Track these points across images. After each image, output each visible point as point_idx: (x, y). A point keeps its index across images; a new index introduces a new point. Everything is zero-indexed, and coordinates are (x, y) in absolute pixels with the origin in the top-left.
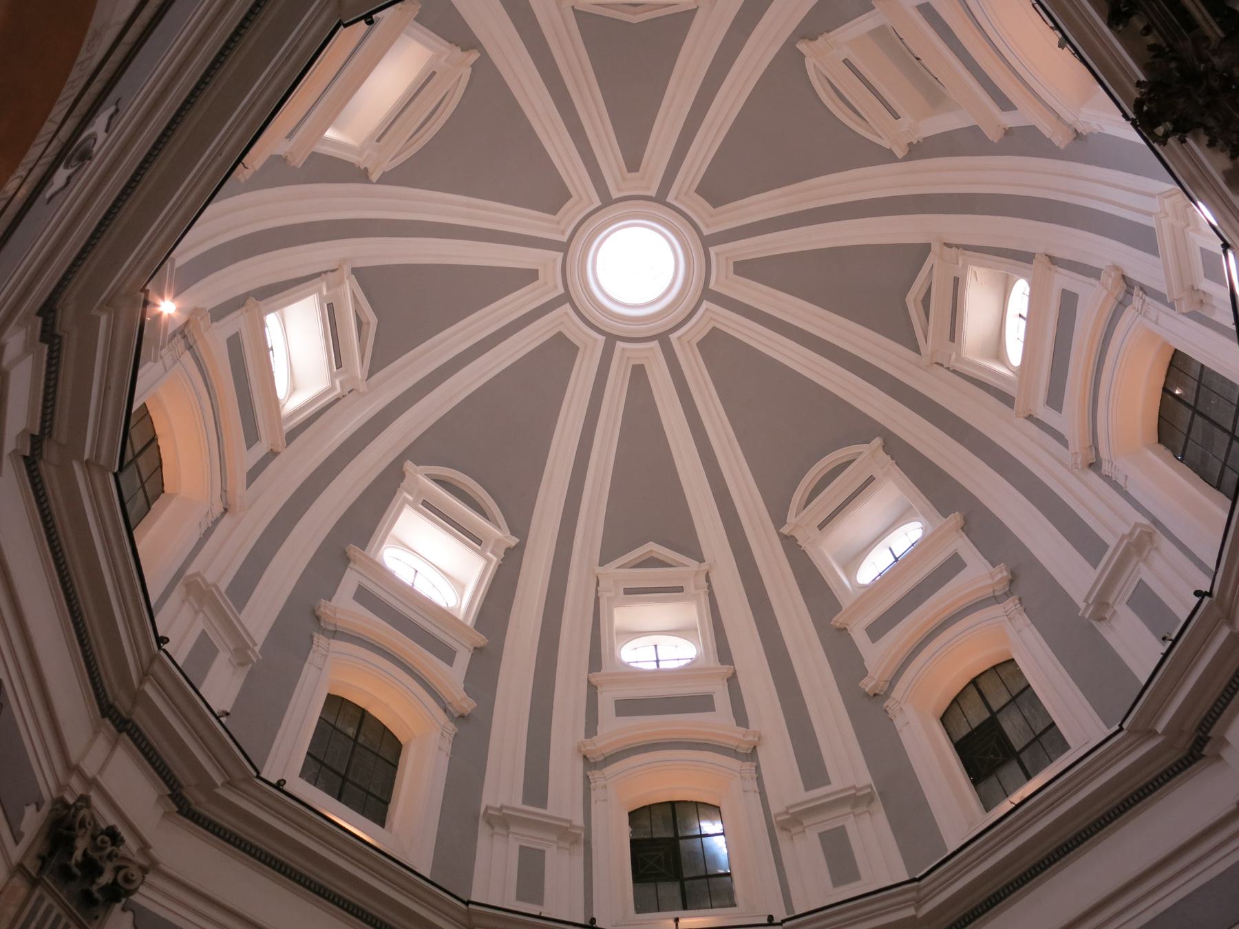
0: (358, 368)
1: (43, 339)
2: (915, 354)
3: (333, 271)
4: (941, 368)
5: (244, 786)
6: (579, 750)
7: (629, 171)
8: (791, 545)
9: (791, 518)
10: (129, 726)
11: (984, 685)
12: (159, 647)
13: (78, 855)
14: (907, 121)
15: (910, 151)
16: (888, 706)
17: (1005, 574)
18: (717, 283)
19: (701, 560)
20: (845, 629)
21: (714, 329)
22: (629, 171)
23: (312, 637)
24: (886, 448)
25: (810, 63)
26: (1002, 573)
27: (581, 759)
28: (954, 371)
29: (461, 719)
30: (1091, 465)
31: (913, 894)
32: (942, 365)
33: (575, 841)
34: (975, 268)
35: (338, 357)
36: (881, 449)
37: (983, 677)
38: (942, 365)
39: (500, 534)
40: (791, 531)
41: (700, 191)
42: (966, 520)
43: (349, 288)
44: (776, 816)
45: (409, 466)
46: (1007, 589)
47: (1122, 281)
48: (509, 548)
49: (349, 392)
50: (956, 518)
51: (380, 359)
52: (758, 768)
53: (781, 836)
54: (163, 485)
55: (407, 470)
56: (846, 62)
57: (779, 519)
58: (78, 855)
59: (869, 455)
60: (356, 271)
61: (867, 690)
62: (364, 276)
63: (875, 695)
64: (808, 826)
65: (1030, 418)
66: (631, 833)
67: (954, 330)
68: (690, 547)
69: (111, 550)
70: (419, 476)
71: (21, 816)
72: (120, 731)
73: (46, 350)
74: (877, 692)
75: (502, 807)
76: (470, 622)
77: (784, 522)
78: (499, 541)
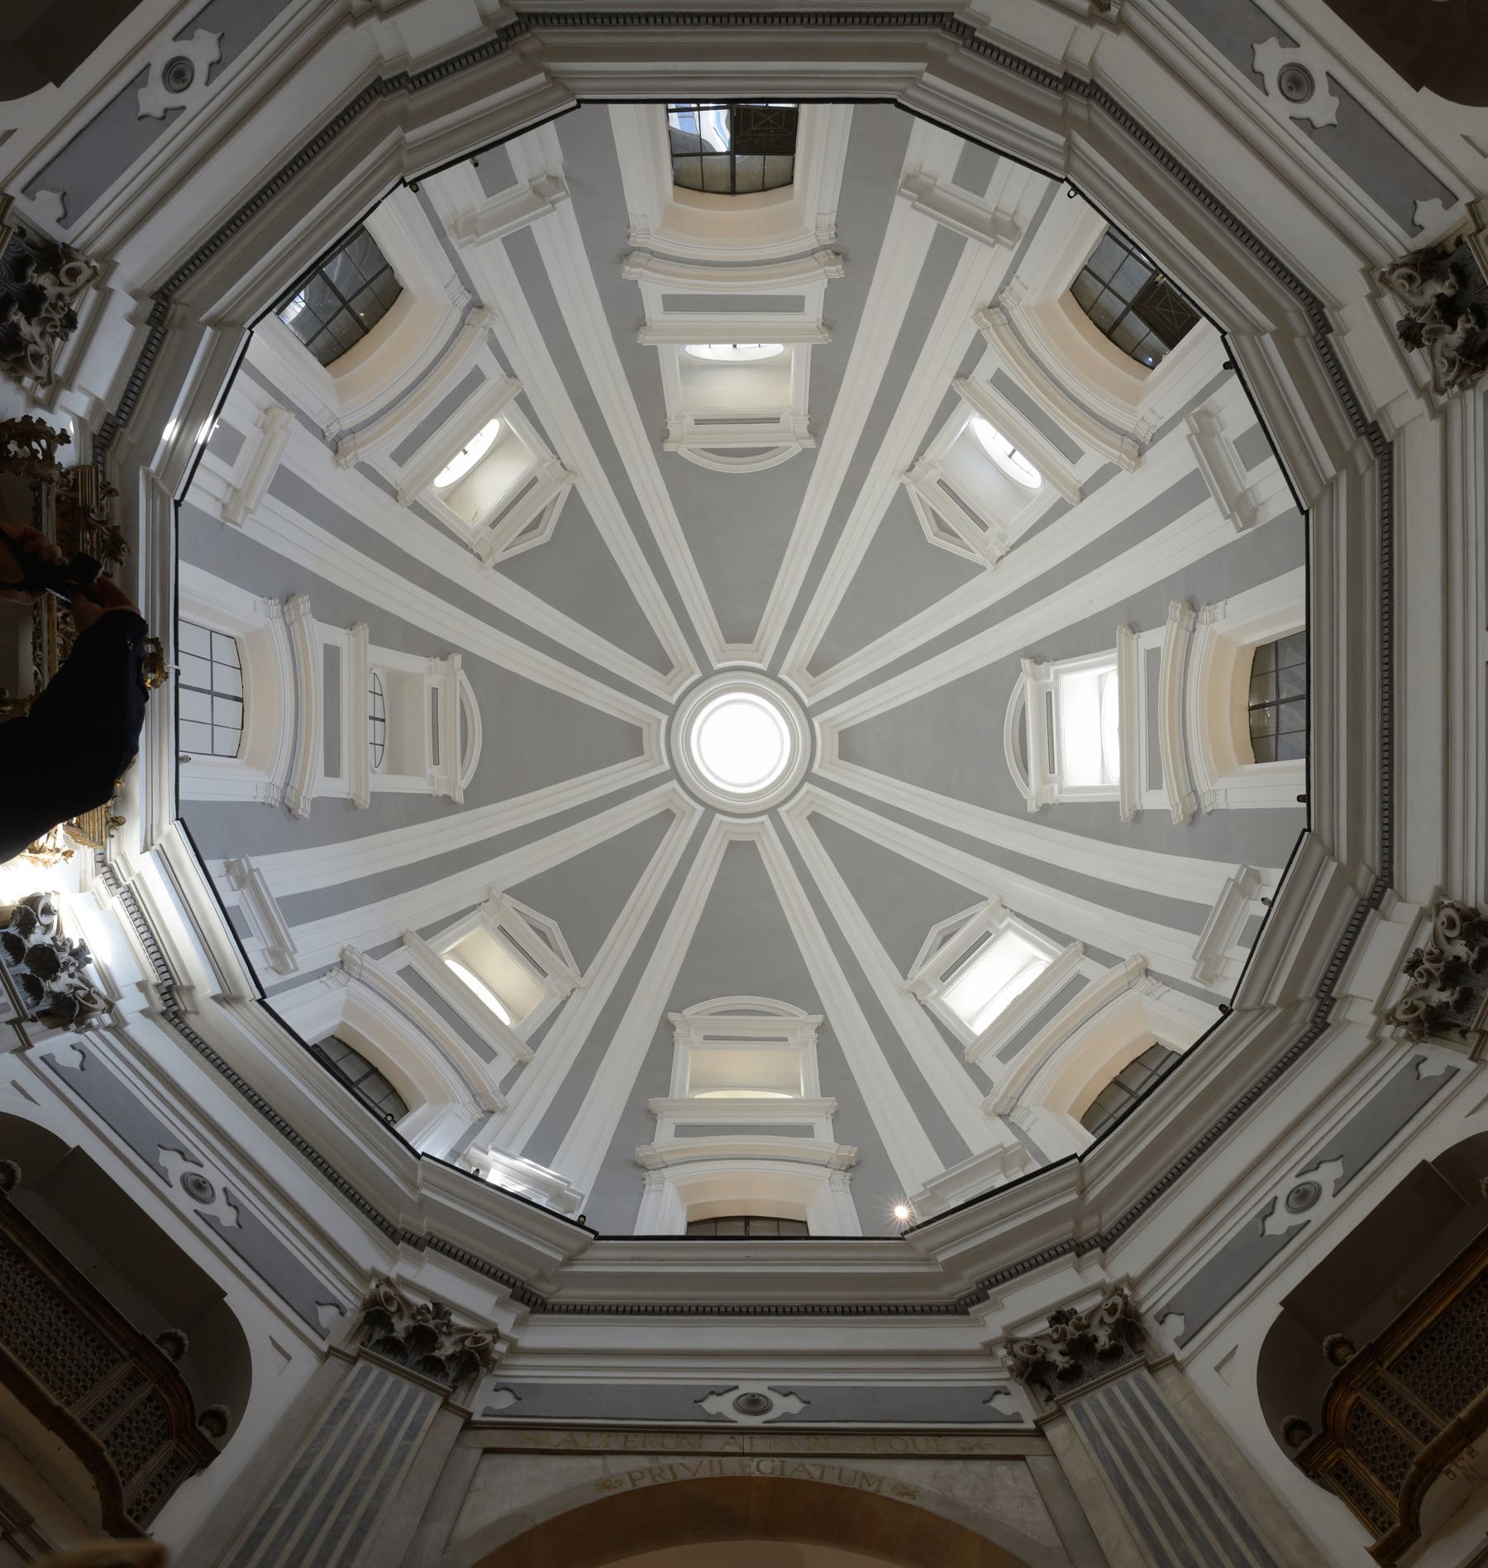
0: (981, 911)
1: (987, 1297)
2: (579, 490)
3: (915, 996)
4: (564, 462)
5: (1326, 837)
6: (1138, 465)
7: (674, 815)
8: (817, 428)
9: (796, 449)
10: (1322, 995)
11: (725, 184)
12: (1232, 1011)
13: (1445, 997)
14: (431, 681)
15: (450, 653)
16: (830, 239)
17: (627, 268)
18: (692, 673)
19: (902, 488)
20: (823, 324)
21: (727, 642)
22: (674, 815)
23: (1209, 814)
24: (665, 435)
25: (464, 783)
26: (629, 272)
27: (1143, 457)
28: (554, 452)
29: (1193, 606)
30: (481, 307)
31: (912, 92)
32: (562, 464)
33: (1206, 413)
34: (469, 524)
35: (982, 940)
36: (670, 439)
37: (721, 190)
38: (562, 464)
39: (1027, 684)
40: (806, 438)
41: (639, 751)
42: (637, 329)
43: (922, 970)
44: (1011, 248)
45: (1032, 807)
46: (635, 253)
47: (339, 450)
48: (1035, 661)
49: (1005, 907)
50: (645, 339)
51: (968, 898)
52: (1001, 291)
53: (1025, 227)
54: (1152, 1048)
55: (1037, 807)
56: (436, 762)
57: (806, 461)
58: (1445, 997)
59: (686, 443)
60: (904, 971)
61: (840, 267)
62: (904, 967)
63: (837, 254)
64: (988, 212)
65: (511, 374)
66: (1165, 354)
67: (529, 485)
68: (901, 507)
69: (1153, 1120)
70: (1033, 792)
71: (1430, 1079)
72: (1334, 1000)
73: (994, 1290)
74: (833, 257)
75: (1227, 517)
76: (1113, 654)
77: (805, 451)
78: (1035, 677)
